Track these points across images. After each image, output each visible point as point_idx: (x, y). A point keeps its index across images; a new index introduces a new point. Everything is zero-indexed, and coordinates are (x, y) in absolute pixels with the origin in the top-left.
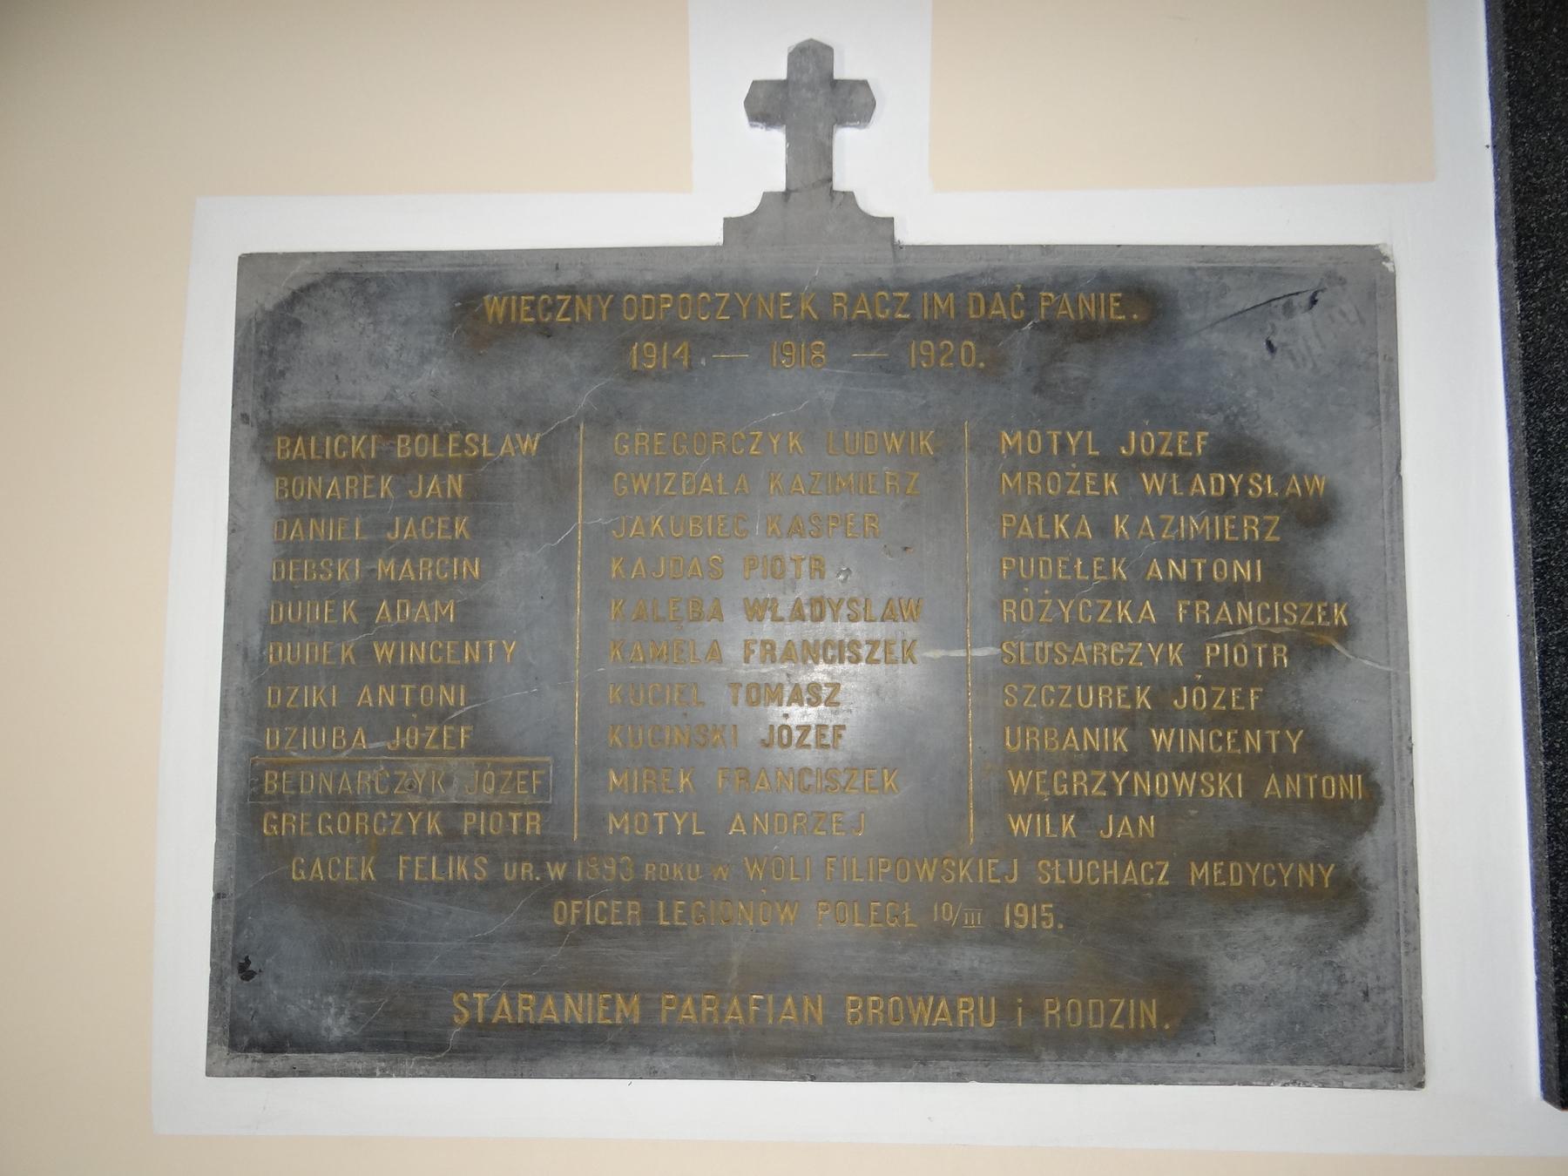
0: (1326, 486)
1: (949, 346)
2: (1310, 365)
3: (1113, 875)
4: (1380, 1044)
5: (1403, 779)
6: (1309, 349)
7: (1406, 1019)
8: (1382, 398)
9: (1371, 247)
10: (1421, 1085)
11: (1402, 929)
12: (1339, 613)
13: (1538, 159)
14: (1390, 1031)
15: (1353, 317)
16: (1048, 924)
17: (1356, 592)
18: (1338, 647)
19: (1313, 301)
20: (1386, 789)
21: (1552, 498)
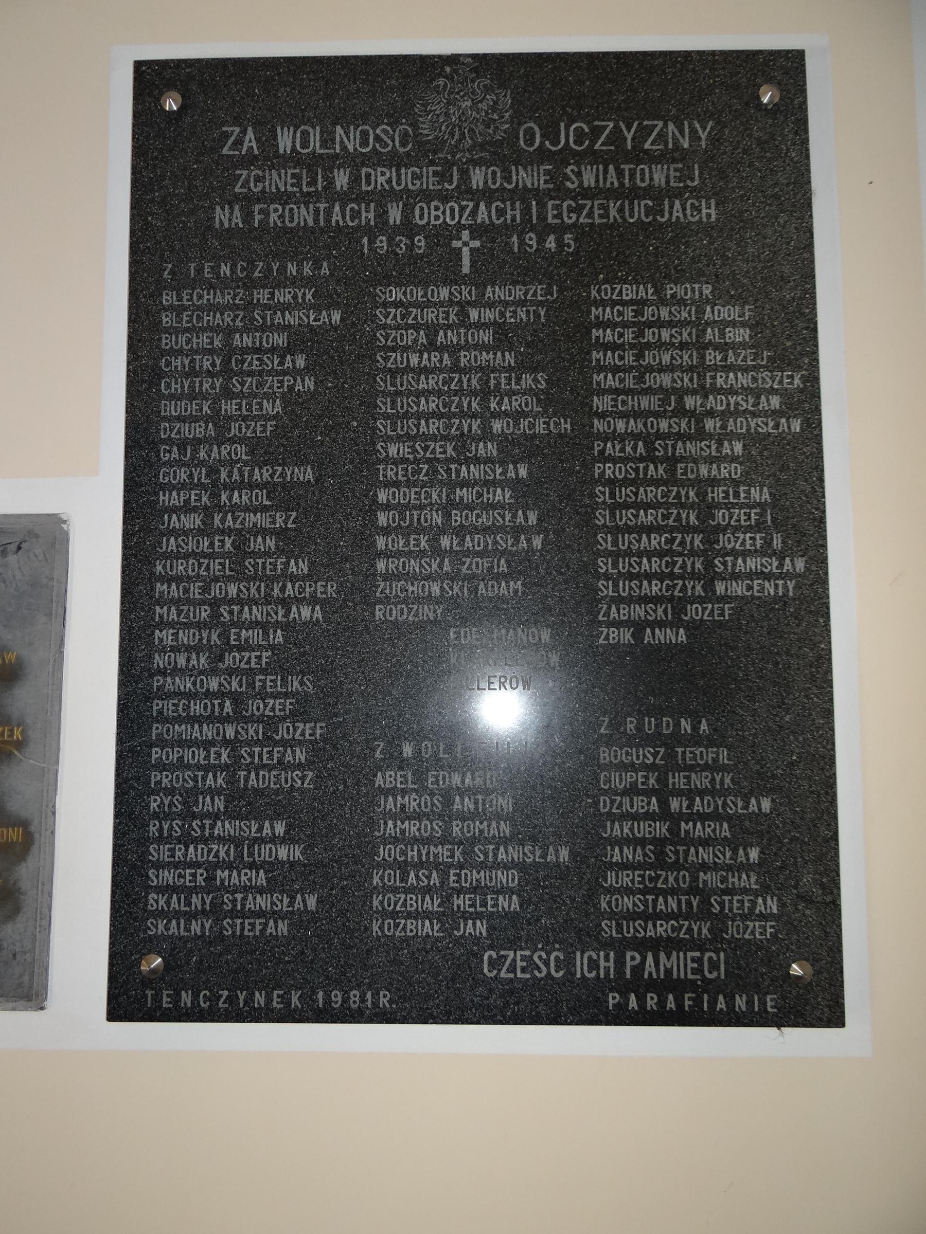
0: (17, 658)
1: (384, 148)
2: (14, 586)
4: (20, 985)
5: (46, 830)
6: (14, 576)
7: (36, 970)
8: (54, 605)
10: (42, 1008)
11: (38, 918)
12: (17, 734)
13: (140, 466)
14: (26, 978)
15: (41, 557)
17: (29, 720)
18: (16, 753)
19: (19, 548)
20: (36, 836)
21: (132, 666)
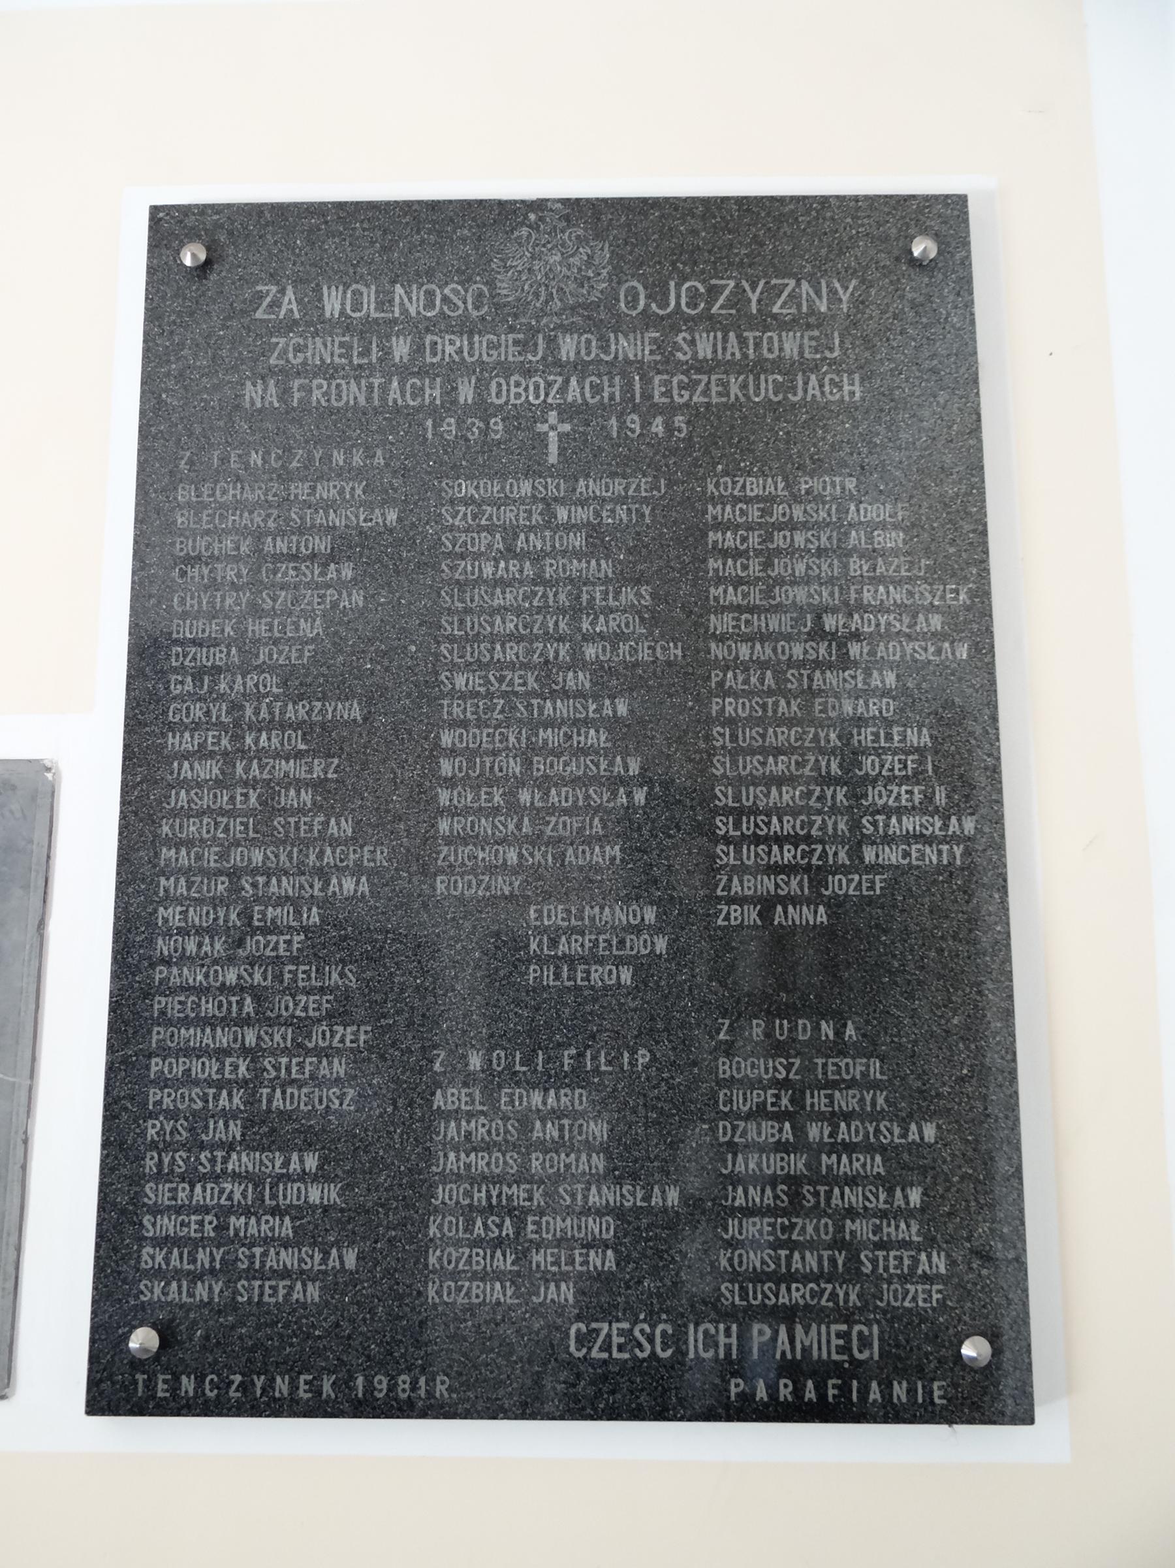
3: (730, 1344)
9: (37, 761)
13: (144, 701)
15: (18, 815)
16: (212, 1380)
21: (128, 953)
